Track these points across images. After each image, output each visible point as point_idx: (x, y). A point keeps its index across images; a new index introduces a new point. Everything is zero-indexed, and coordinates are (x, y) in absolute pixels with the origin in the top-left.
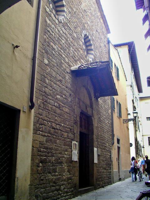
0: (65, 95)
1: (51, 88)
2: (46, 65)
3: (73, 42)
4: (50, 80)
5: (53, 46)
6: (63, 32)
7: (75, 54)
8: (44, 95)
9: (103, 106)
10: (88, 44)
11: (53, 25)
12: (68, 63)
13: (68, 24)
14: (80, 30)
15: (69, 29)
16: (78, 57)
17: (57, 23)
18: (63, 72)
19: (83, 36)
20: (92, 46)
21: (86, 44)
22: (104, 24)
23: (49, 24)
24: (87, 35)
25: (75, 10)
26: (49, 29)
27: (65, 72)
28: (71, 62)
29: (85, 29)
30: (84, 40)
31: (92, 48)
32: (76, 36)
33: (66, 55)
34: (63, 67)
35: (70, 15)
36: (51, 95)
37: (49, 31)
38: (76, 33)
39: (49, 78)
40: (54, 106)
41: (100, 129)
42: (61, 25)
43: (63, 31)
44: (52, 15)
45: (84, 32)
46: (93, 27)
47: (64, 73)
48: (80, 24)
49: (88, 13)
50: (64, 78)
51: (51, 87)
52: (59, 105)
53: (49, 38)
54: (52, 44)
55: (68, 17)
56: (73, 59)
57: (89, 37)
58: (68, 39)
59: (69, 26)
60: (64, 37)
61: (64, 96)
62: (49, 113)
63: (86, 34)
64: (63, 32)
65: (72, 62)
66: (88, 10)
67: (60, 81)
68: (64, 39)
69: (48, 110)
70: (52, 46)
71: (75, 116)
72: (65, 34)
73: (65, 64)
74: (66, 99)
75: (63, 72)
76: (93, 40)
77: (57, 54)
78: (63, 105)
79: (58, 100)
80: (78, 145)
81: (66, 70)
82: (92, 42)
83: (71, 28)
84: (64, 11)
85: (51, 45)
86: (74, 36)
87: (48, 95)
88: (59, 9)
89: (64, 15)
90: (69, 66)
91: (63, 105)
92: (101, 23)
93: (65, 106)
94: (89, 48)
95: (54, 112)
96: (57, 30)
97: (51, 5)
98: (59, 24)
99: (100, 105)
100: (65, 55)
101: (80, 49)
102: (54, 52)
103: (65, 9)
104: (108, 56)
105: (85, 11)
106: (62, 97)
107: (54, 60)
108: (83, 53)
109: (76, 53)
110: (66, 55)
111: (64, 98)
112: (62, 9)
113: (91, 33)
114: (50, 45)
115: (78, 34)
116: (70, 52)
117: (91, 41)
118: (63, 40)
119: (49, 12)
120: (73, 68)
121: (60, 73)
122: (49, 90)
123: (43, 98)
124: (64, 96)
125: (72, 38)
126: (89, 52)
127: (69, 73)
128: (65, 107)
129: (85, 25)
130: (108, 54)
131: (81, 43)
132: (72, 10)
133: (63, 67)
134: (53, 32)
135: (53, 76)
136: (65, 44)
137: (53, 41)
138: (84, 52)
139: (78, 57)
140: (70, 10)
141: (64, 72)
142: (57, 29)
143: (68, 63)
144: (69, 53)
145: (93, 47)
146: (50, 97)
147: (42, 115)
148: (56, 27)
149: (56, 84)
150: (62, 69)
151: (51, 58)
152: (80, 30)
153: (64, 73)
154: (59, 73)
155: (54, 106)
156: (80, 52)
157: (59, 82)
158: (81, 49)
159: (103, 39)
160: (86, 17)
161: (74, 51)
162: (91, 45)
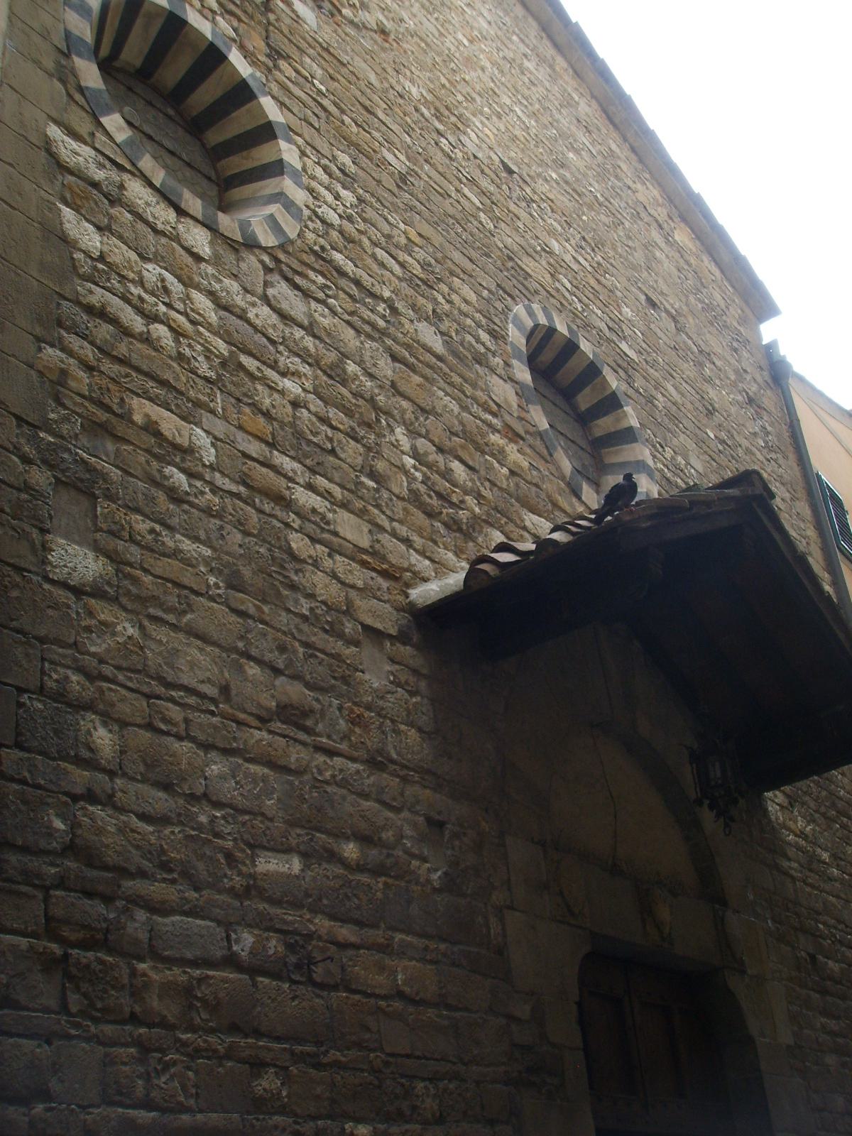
0: (365, 840)
1: (160, 801)
2: (78, 591)
3: (403, 386)
4: (150, 727)
5: (169, 423)
6: (283, 316)
7: (447, 474)
8: (62, 883)
9: (825, 856)
10: (585, 400)
11: (150, 266)
12: (374, 554)
13: (338, 257)
14: (472, 297)
15: (354, 291)
16: (479, 496)
17: (206, 251)
18: (319, 638)
19: (516, 337)
20: (628, 409)
21: (574, 407)
22: (705, 258)
23: (102, 258)
24: (562, 328)
25: (398, 162)
26: (98, 296)
27: (340, 635)
28: (407, 542)
29: (529, 295)
30: (532, 361)
31: (624, 425)
32: (438, 345)
33: (337, 492)
34: (311, 596)
35: (344, 193)
36: (165, 866)
37: (101, 313)
38: (435, 318)
39: (130, 706)
40: (231, 961)
41: (831, 1060)
42: (251, 262)
43: (284, 306)
44: (136, 191)
45: (519, 309)
46: (609, 280)
47: (338, 646)
48: (474, 254)
49: (542, 187)
50: (346, 677)
51: (167, 787)
52: (296, 940)
53: (108, 366)
54: (142, 409)
55: (323, 210)
56: (431, 514)
57: (585, 346)
58: (351, 367)
59: (349, 267)
60: (304, 355)
61: (350, 850)
62: (145, 1048)
63: (551, 331)
64: (283, 316)
65: (418, 541)
66: (542, 163)
67: (292, 715)
68: (305, 369)
69: (134, 1019)
70: (152, 428)
71: (523, 1010)
72: (310, 329)
73: (340, 564)
74: (378, 871)
75: (319, 638)
76: (625, 367)
77: (215, 490)
78: (346, 933)
79: (277, 902)
80: (335, 747)
81: (349, 611)
82: (614, 382)
83: (367, 280)
84: (278, 168)
85: (138, 418)
86: (415, 345)
87: (123, 872)
88: (237, 163)
89: (280, 197)
90: (385, 574)
91: (346, 933)
92: (680, 250)
93: (377, 935)
94: (604, 425)
95: (234, 1028)
96: (202, 302)
97: (114, 122)
98: (230, 257)
99: (791, 852)
100: (325, 495)
101: (495, 438)
102: (180, 479)
103: (288, 152)
104: (796, 468)
105: (511, 172)
106: (333, 856)
107: (187, 545)
108: (541, 465)
109: (456, 466)
110: (337, 492)
111: (360, 868)
112: (263, 154)
113: (597, 316)
114: (126, 417)
115: (462, 329)
116: (380, 466)
117: (607, 372)
118: (296, 374)
119: (93, 167)
120: (429, 591)
121: (282, 649)
122: (143, 817)
123: (58, 912)
124: (350, 850)
125: (395, 358)
126: (608, 460)
127: (402, 638)
128: (385, 949)
129: (528, 265)
130: (792, 456)
131: (504, 392)
132: (364, 161)
133: (311, 596)
134: (152, 318)
135: (185, 679)
136: (316, 404)
137: (164, 383)
138: (549, 458)
139: (479, 496)
140: (345, 159)
141: (334, 631)
142: (211, 294)
143: (371, 558)
144: (373, 475)
145: (631, 416)
146: (157, 889)
147: (46, 1095)
148: (187, 283)
149: (227, 752)
150: (305, 607)
151: (142, 525)
152: (472, 297)
153: (338, 646)
154: (263, 648)
155: (231, 961)
156: (500, 455)
157: (277, 726)
158: (514, 436)
159: (727, 354)
160: (523, 214)
161: (434, 457)
162: (612, 403)
